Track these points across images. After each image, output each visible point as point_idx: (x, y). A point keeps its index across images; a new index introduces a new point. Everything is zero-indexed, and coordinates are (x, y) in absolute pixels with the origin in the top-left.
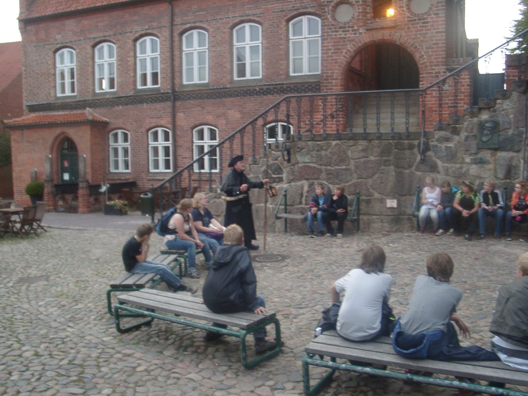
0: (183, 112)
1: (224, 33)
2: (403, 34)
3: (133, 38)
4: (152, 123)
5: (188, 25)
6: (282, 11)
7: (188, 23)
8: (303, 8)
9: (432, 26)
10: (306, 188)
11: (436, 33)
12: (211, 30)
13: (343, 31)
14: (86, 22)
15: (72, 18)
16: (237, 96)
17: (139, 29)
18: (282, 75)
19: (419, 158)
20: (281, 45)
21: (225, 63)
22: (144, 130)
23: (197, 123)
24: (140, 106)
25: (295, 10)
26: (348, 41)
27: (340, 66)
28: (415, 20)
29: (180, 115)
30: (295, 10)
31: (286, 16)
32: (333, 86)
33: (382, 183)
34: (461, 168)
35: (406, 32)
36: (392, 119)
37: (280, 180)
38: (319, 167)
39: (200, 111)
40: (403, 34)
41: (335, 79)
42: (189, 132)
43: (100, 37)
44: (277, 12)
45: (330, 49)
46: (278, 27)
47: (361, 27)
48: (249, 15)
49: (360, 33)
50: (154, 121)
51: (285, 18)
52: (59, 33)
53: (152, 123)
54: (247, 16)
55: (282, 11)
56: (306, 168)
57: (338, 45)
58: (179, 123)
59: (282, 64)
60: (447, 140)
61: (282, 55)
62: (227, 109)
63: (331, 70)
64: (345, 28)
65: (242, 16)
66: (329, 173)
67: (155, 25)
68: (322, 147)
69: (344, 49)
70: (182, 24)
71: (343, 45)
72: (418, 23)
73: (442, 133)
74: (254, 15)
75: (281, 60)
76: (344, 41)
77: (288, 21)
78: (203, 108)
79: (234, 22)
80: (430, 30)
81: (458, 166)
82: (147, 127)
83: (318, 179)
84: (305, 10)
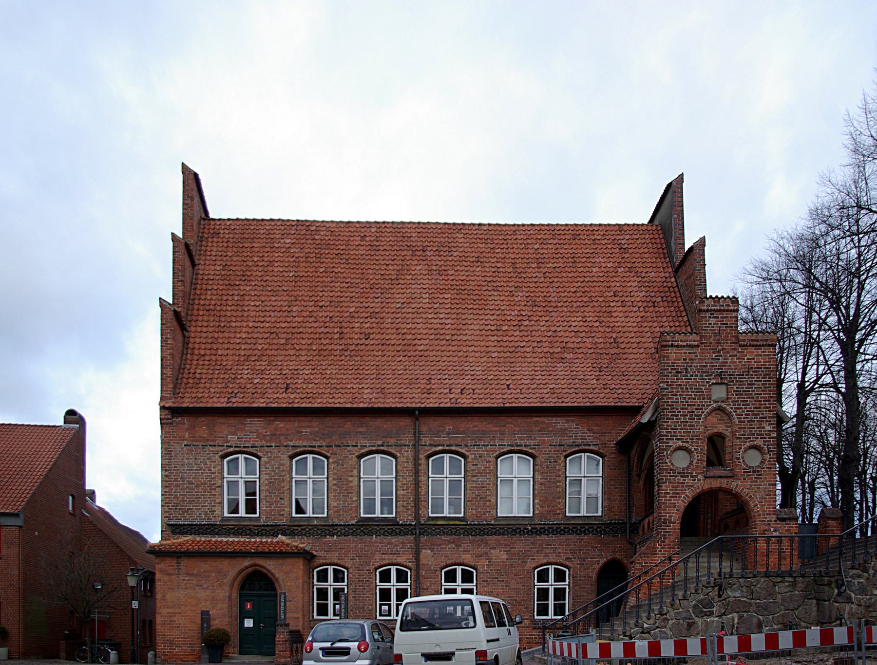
0: (430, 549)
1: (489, 462)
2: (740, 483)
3: (357, 454)
4: (384, 559)
5: (440, 448)
6: (559, 445)
7: (439, 445)
8: (585, 445)
9: (766, 478)
10: (736, 621)
11: (769, 485)
12: (471, 457)
13: (681, 477)
14: (281, 424)
15: (258, 417)
16: (503, 534)
17: (368, 445)
18: (559, 514)
19: (836, 591)
20: (559, 482)
21: (490, 495)
22: (372, 568)
23: (449, 562)
24: (367, 538)
25: (576, 445)
26: (686, 486)
27: (678, 510)
28: (750, 472)
29: (426, 553)
30: (576, 445)
31: (565, 451)
32: (670, 529)
33: (806, 613)
34: (870, 599)
35: (742, 482)
36: (709, 563)
37: (711, 613)
38: (748, 601)
39: (454, 548)
40: (740, 483)
41: (672, 523)
42: (438, 573)
43: (305, 446)
44: (556, 445)
45: (669, 493)
46: (555, 462)
47: (700, 473)
48: (521, 446)
49: (699, 480)
50: (387, 558)
51: (564, 454)
52: (235, 434)
53: (384, 559)
54: (518, 446)
55: (559, 445)
56: (737, 600)
57: (677, 490)
58: (423, 561)
59: (559, 503)
60: (859, 576)
61: (559, 492)
62: (490, 549)
63: (669, 513)
64: (684, 473)
65: (512, 446)
66: (758, 606)
67: (392, 441)
68: (752, 583)
69: (682, 494)
70: (431, 445)
71: (682, 490)
72: (753, 475)
73: (855, 571)
74: (526, 446)
75: (559, 498)
76: (683, 487)
77: (566, 457)
78: (458, 546)
79: (502, 451)
80: (763, 481)
81: (868, 597)
82: (377, 565)
83: (749, 611)
84: (587, 448)
